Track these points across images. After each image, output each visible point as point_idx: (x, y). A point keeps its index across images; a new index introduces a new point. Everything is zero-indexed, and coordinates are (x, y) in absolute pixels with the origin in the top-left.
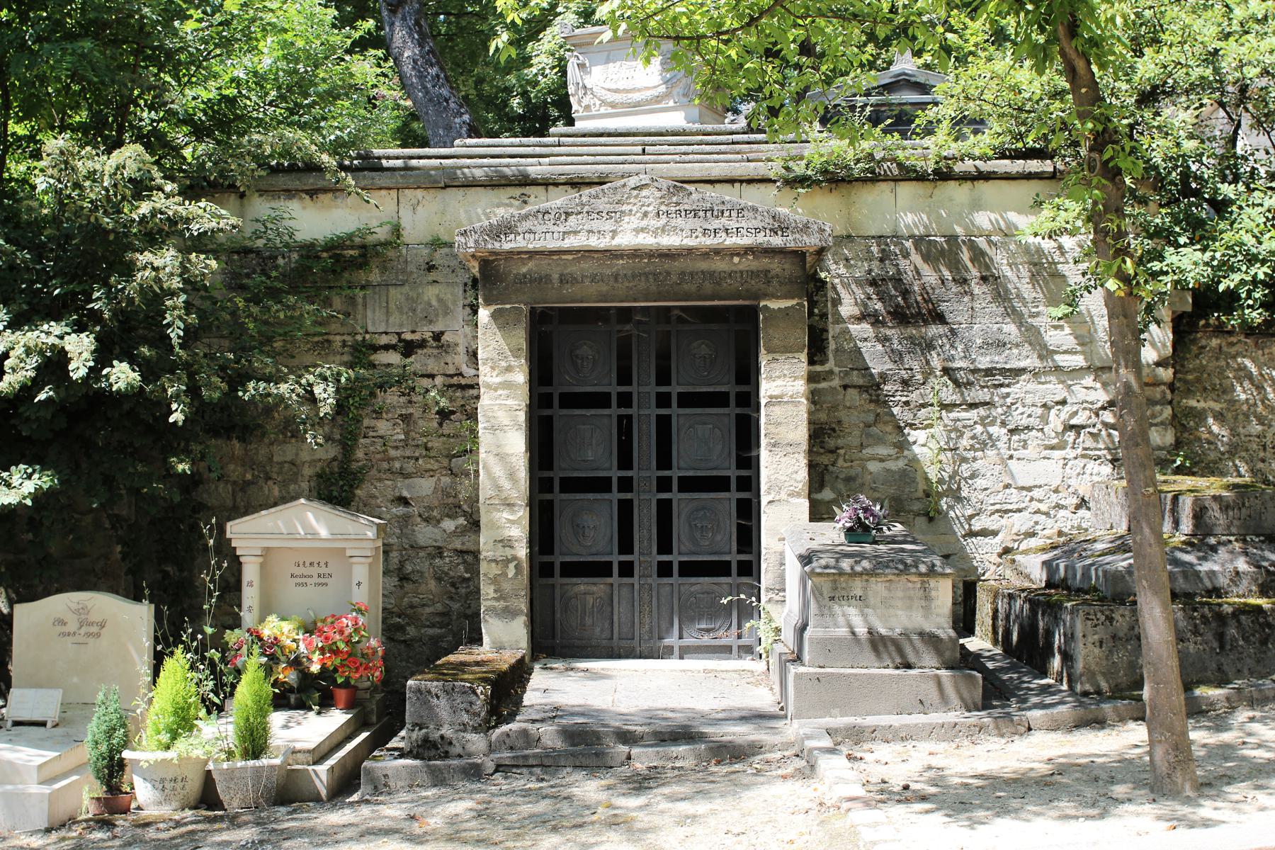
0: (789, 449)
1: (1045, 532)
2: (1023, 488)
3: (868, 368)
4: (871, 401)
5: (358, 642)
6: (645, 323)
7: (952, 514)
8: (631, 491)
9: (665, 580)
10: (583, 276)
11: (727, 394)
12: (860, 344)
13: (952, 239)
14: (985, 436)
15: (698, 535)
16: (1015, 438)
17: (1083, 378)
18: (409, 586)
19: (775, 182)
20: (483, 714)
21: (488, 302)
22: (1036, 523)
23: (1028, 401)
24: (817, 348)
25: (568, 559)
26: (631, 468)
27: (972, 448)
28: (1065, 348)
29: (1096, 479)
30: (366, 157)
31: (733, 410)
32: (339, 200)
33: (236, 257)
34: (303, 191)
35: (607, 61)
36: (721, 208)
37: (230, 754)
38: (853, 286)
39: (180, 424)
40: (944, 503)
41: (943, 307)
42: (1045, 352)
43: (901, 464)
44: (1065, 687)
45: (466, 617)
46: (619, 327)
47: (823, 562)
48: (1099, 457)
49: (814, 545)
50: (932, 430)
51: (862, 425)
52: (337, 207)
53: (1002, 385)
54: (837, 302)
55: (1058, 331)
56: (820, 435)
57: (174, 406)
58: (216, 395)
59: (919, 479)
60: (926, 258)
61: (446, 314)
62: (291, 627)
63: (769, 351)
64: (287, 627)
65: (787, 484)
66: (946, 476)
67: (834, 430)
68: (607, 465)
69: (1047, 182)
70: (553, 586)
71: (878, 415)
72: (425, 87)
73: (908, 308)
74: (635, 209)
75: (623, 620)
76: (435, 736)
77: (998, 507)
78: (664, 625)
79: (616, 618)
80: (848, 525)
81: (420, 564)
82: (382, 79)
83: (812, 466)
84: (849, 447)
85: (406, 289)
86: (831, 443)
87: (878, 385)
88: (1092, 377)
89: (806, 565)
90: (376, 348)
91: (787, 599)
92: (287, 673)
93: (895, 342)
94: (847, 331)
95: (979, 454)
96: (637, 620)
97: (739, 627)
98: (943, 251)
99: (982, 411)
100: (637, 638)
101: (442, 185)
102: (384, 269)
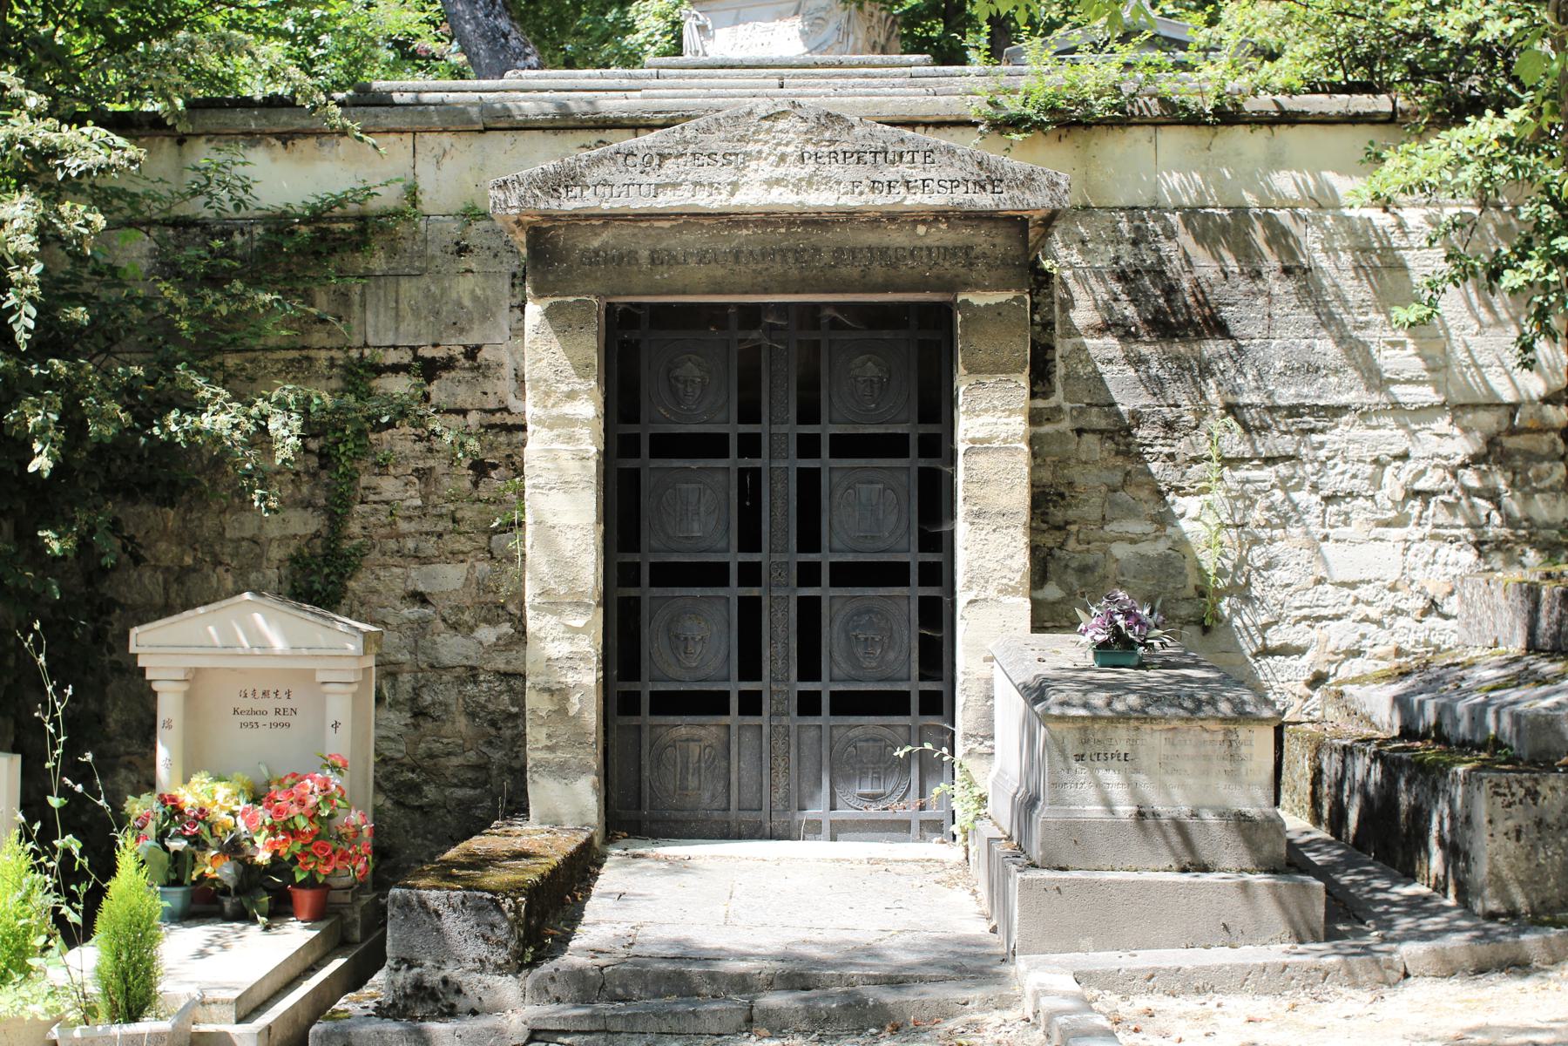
0: (1001, 521)
1: (1377, 650)
2: (1343, 584)
3: (1113, 404)
4: (1118, 453)
5: (331, 816)
6: (782, 328)
7: (1237, 622)
8: (759, 584)
11: (904, 438)
12: (1101, 368)
13: (1240, 211)
14: (1287, 507)
15: (860, 651)
16: (1333, 509)
17: (1433, 420)
18: (428, 725)
19: (976, 125)
20: (512, 944)
21: (540, 293)
22: (1363, 636)
23: (1353, 453)
24: (1040, 375)
25: (661, 687)
27: (1268, 524)
28: (1407, 375)
29: (1452, 570)
30: (364, 89)
31: (914, 462)
32: (326, 149)
33: (171, 232)
34: (271, 134)
35: (736, 22)
36: (898, 148)
37: (89, 1013)
38: (1092, 281)
39: (46, 475)
40: (1225, 606)
41: (1227, 313)
42: (1375, 379)
43: (1162, 547)
44: (1451, 901)
45: (511, 770)
46: (741, 335)
47: (1061, 697)
48: (1457, 539)
49: (1045, 670)
50: (1209, 497)
51: (1104, 489)
52: (323, 159)
53: (1312, 431)
54: (1067, 305)
55: (1397, 351)
56: (1047, 503)
57: (37, 447)
58: (110, 431)
59: (1189, 569)
60: (1200, 239)
61: (484, 318)
62: (228, 791)
63: (972, 370)
64: (222, 790)
65: (997, 575)
66: (1229, 564)
67: (1062, 496)
68: (722, 544)
69: (1382, 127)
70: (639, 728)
71: (1128, 474)
72: (475, 18)
73: (1174, 314)
75: (745, 780)
76: (433, 979)
77: (1306, 612)
78: (806, 788)
79: (734, 777)
80: (1100, 638)
81: (444, 693)
82: (426, 27)
83: (1034, 549)
84: (1084, 521)
85: (426, 279)
86: (1058, 515)
87: (1128, 430)
88: (1448, 419)
89: (1036, 701)
90: (379, 370)
91: (996, 751)
92: (218, 864)
93: (1155, 365)
94: (1081, 349)
95: (1278, 533)
96: (766, 781)
97: (922, 794)
98: (1226, 229)
99: (1283, 469)
100: (766, 808)
101: (480, 127)
102: (392, 251)
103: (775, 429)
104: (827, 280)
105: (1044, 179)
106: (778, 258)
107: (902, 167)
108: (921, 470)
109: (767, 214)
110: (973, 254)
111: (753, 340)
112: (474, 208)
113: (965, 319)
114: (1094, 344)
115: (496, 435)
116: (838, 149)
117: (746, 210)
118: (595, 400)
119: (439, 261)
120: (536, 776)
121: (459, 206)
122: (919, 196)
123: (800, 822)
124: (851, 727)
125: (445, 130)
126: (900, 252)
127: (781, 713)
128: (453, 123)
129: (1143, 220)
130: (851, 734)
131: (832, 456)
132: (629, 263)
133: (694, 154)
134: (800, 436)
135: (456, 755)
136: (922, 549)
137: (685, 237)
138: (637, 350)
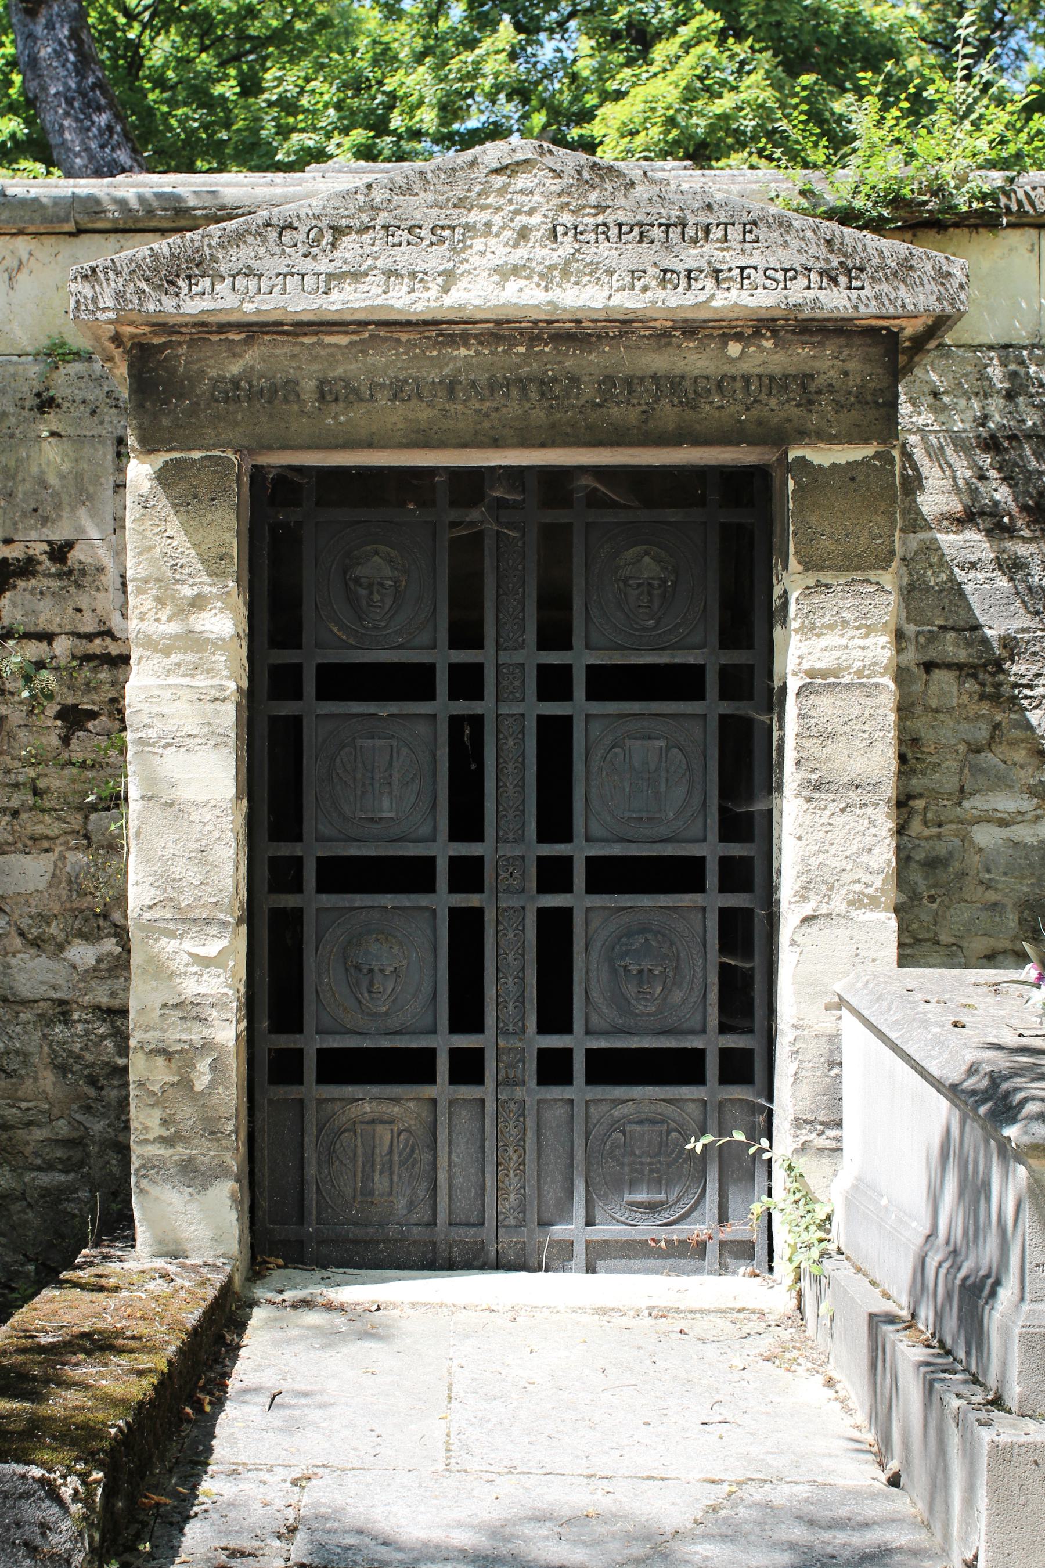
0: (853, 796)
3: (976, 627)
4: (983, 697)
6: (515, 506)
9: (556, 1092)
10: (373, 386)
12: (960, 575)
15: (630, 990)
26: (479, 837)
36: (703, 219)
38: (949, 451)
46: (453, 515)
51: (962, 748)
63: (809, 565)
65: (846, 878)
68: (425, 830)
71: (997, 726)
72: (87, 149)
74: (498, 220)
75: (458, 1181)
79: (442, 1177)
84: (935, 794)
91: (845, 1145)
94: (932, 548)
101: (70, 227)
103: (504, 657)
104: (590, 428)
105: (928, 267)
106: (514, 392)
107: (708, 249)
108: (723, 718)
109: (498, 322)
110: (813, 388)
111: (472, 524)
112: (63, 344)
113: (800, 487)
114: (949, 540)
115: (95, 670)
116: (610, 220)
117: (467, 314)
118: (234, 610)
119: (13, 420)
120: (144, 1183)
121: (44, 342)
122: (734, 292)
123: (541, 1245)
124: (616, 1103)
125: (21, 232)
126: (702, 384)
127: (510, 1085)
128: (32, 221)
129: (1022, 363)
130: (616, 1113)
131: (589, 698)
132: (286, 400)
133: (385, 227)
134: (542, 668)
135: (39, 1125)
136: (724, 838)
137: (371, 360)
138: (295, 542)
